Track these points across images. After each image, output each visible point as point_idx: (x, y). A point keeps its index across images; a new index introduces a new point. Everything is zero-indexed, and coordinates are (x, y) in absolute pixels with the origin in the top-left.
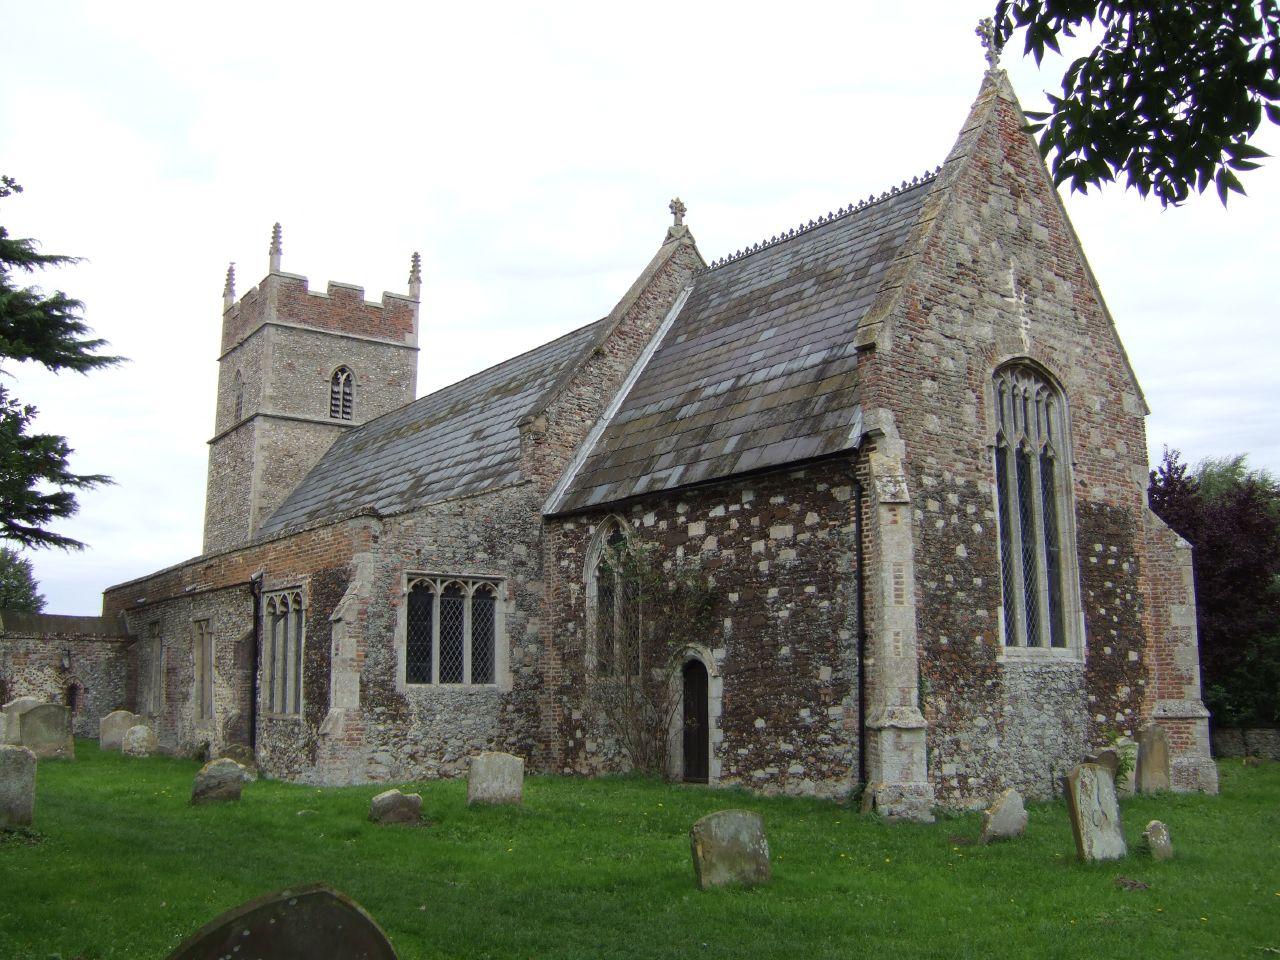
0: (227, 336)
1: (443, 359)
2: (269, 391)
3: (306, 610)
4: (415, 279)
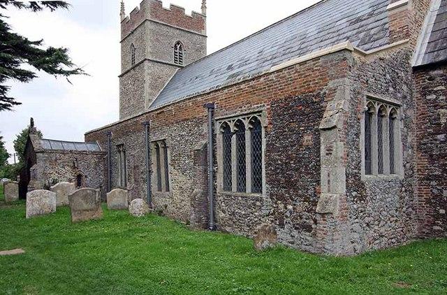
0: (123, 31)
1: (216, 37)
2: (149, 50)
3: (266, 127)
4: (204, 7)
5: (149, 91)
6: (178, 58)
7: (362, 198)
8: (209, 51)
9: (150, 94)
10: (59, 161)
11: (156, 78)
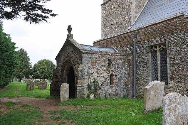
5: (135, 10)
7: (109, 60)
9: (136, 12)
10: (98, 62)
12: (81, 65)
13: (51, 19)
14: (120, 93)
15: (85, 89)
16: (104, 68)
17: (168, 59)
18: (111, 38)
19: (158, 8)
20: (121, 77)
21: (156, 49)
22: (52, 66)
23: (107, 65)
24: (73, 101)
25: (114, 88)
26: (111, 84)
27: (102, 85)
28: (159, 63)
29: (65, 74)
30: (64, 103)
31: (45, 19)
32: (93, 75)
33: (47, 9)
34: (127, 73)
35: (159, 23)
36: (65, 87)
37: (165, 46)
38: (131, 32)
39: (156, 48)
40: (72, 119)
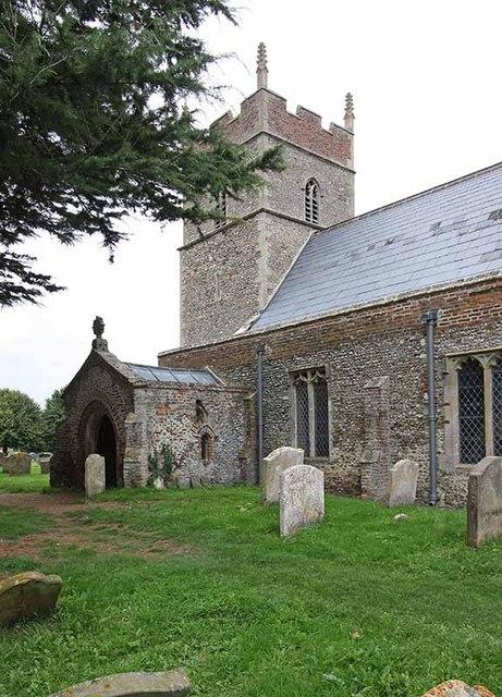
1: (376, 181)
4: (349, 116)
5: (268, 271)
6: (312, 209)
7: (198, 402)
8: (361, 206)
9: (270, 279)
11: (279, 248)
12: (131, 415)
13: (47, 297)
14: (225, 476)
15: (142, 468)
16: (187, 421)
17: (330, 403)
18: (204, 347)
19: (325, 273)
20: (229, 442)
21: (305, 380)
22: (29, 411)
23: (194, 413)
24: (114, 494)
25: (212, 465)
26: (203, 457)
27: (183, 458)
28: (312, 409)
29: (88, 434)
30: (94, 498)
31: (31, 296)
32: (160, 436)
33: (37, 273)
34: (242, 431)
35: (311, 322)
36: (95, 463)
37: (323, 372)
38: (252, 336)
39: (306, 376)
40: (121, 522)
